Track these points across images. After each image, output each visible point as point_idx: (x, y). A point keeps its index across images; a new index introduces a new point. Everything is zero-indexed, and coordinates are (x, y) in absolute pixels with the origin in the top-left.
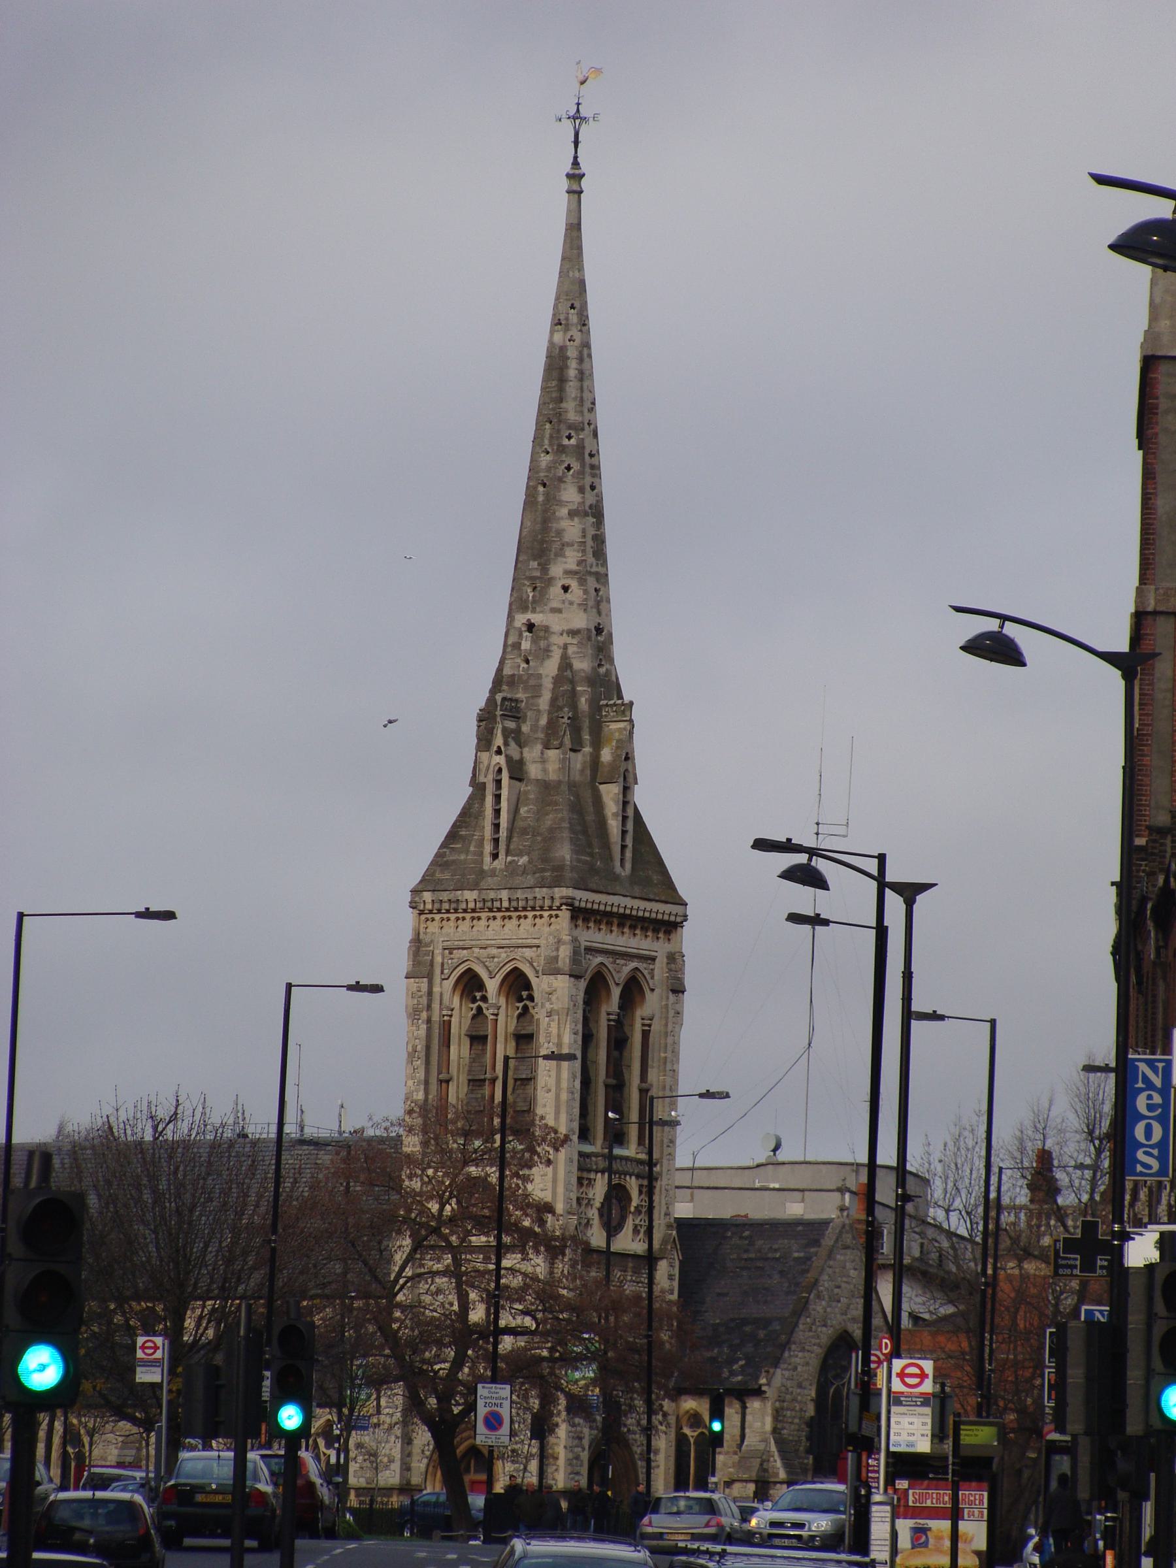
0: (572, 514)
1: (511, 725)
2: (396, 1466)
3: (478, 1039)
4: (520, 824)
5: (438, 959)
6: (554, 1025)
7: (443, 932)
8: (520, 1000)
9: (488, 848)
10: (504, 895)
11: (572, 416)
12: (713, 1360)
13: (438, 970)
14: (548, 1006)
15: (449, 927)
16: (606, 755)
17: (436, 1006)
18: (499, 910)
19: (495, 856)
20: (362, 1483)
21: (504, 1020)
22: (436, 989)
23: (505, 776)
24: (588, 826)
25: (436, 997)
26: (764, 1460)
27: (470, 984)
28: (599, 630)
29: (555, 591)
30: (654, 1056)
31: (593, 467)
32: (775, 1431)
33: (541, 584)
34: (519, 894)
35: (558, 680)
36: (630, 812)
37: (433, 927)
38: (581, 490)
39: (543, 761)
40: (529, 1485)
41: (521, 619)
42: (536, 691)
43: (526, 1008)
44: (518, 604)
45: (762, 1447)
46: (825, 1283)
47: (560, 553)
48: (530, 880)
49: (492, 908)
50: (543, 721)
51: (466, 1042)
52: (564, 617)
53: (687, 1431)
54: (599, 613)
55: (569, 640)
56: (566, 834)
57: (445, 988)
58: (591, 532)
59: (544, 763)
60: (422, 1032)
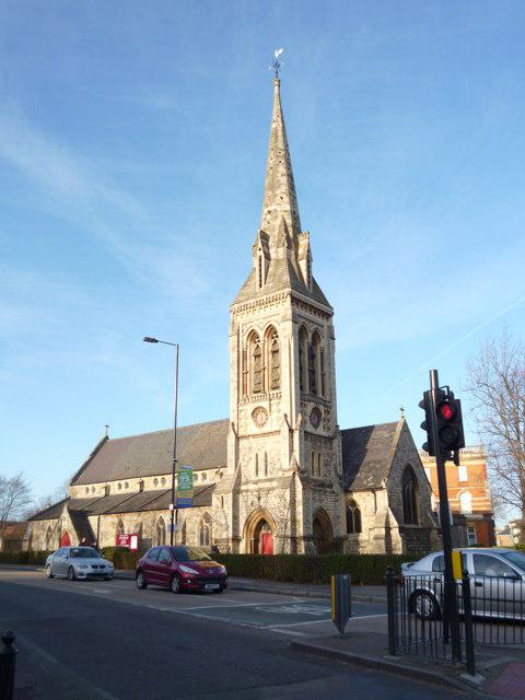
7: (240, 319)
9: (258, 283)
27: (253, 336)
30: (326, 365)
39: (277, 252)
49: (260, 304)
51: (253, 358)
57: (244, 338)
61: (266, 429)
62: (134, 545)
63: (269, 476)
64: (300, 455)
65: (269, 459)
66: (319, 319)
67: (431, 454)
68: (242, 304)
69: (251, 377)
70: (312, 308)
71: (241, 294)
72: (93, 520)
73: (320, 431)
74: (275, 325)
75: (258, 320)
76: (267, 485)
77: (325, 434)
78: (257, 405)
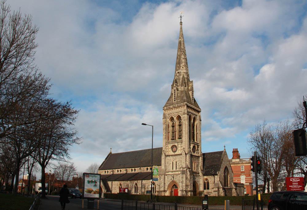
0: (183, 59)
1: (176, 84)
2: (163, 188)
3: (173, 126)
4: (178, 96)
5: (167, 116)
6: (185, 122)
7: (167, 112)
8: (179, 120)
9: (174, 100)
10: (176, 105)
11: (183, 48)
12: (209, 171)
13: (167, 118)
14: (184, 119)
15: (169, 112)
16: (190, 88)
17: (167, 122)
18: (176, 107)
19: (175, 101)
20: (158, 190)
21: (177, 123)
22: (167, 120)
23: (176, 90)
24: (188, 97)
25: (167, 121)
26: (218, 184)
27: (172, 119)
29: (181, 68)
32: (220, 180)
33: (179, 67)
34: (179, 104)
35: (182, 78)
37: (166, 112)
40: (254, 195)
41: (177, 72)
42: (180, 80)
43: (180, 121)
44: (176, 70)
45: (218, 183)
46: (224, 159)
47: (182, 63)
50: (181, 83)
52: (183, 71)
53: (205, 181)
56: (185, 96)
57: (168, 120)
58: (186, 61)
59: (181, 88)
60: (165, 126)
61: (176, 153)
62: (126, 191)
63: (177, 170)
64: (189, 163)
65: (177, 164)
66: (196, 113)
67: (254, 172)
68: (168, 107)
69: (171, 134)
70: (193, 109)
71: (167, 103)
72: (110, 183)
73: (195, 154)
74: (181, 115)
75: (174, 112)
76: (177, 173)
77: (197, 155)
78: (173, 144)
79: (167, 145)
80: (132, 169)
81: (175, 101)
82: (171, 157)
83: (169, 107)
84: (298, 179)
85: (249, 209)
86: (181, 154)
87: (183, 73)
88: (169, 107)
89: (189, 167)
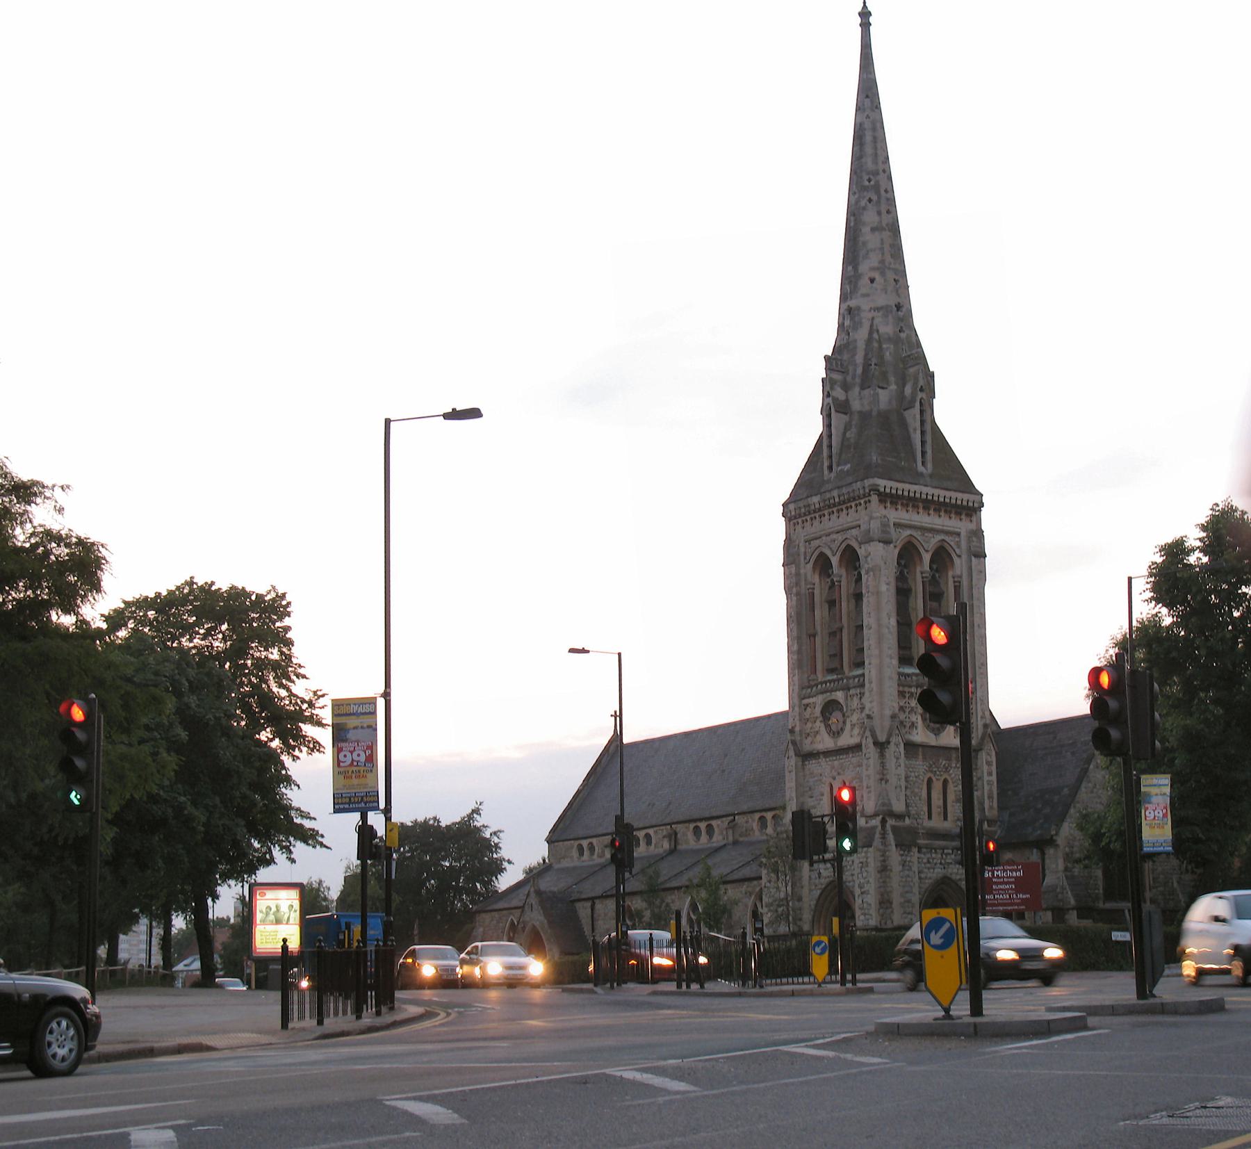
0: (873, 230)
5: (802, 550)
10: (835, 493)
18: (834, 505)
19: (830, 468)
22: (802, 571)
28: (899, 307)
29: (865, 281)
31: (888, 199)
34: (844, 490)
35: (869, 341)
36: (928, 427)
38: (879, 213)
47: (866, 256)
48: (850, 479)
54: (898, 295)
55: (876, 314)
74: (855, 544)
79: (806, 701)
80: (591, 843)
81: (830, 468)
82: (822, 760)
83: (805, 502)
84: (1016, 871)
85: (1249, 1003)
86: (858, 747)
87: (873, 314)
88: (805, 502)
89: (899, 807)
